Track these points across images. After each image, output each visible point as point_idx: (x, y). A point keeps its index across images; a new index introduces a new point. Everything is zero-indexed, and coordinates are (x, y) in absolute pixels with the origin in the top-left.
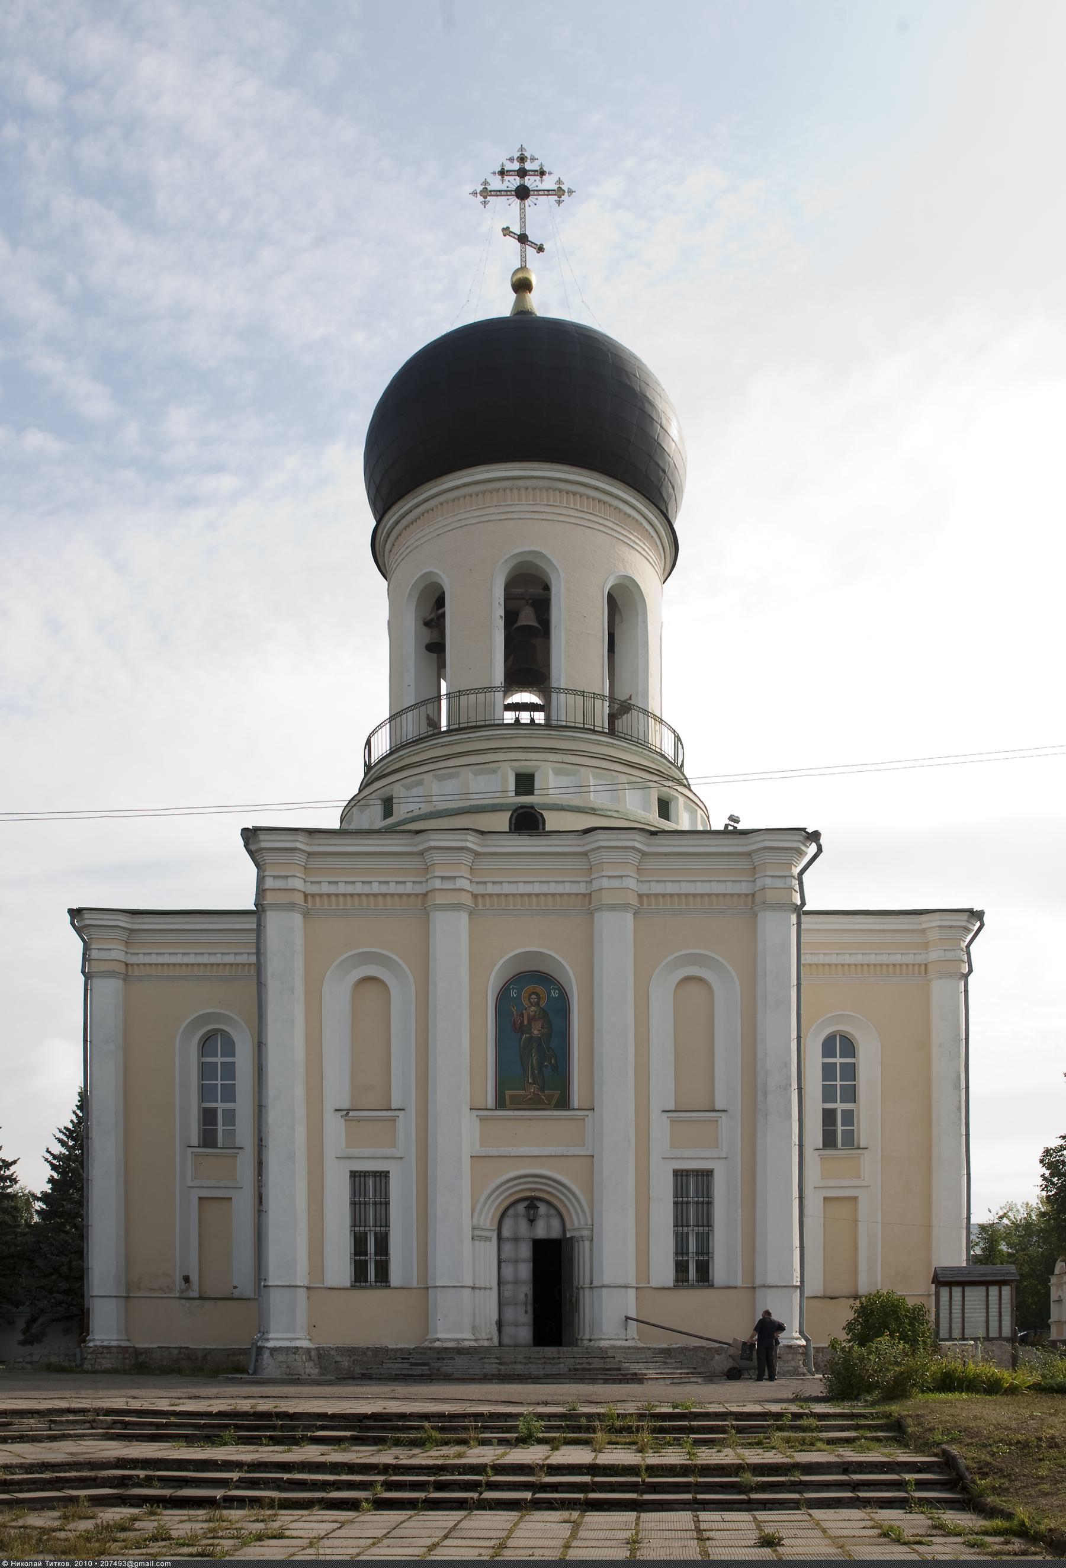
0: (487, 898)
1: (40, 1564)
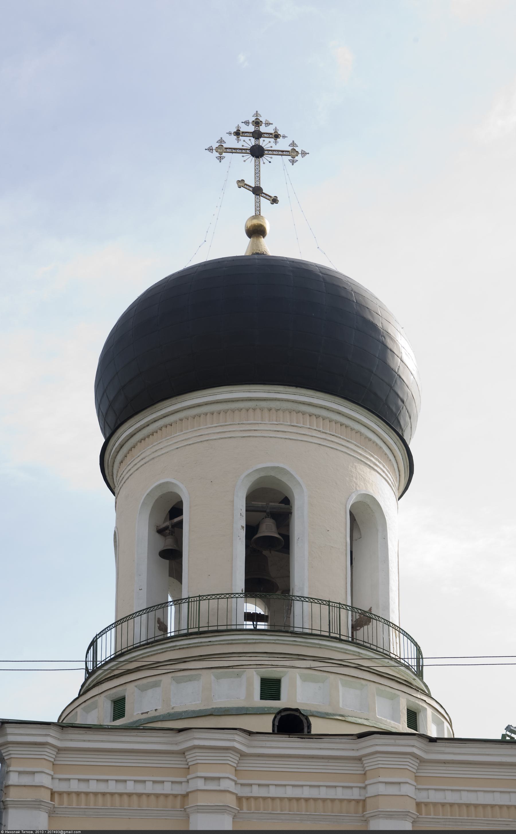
0: (252, 801)
1: (19, 832)
